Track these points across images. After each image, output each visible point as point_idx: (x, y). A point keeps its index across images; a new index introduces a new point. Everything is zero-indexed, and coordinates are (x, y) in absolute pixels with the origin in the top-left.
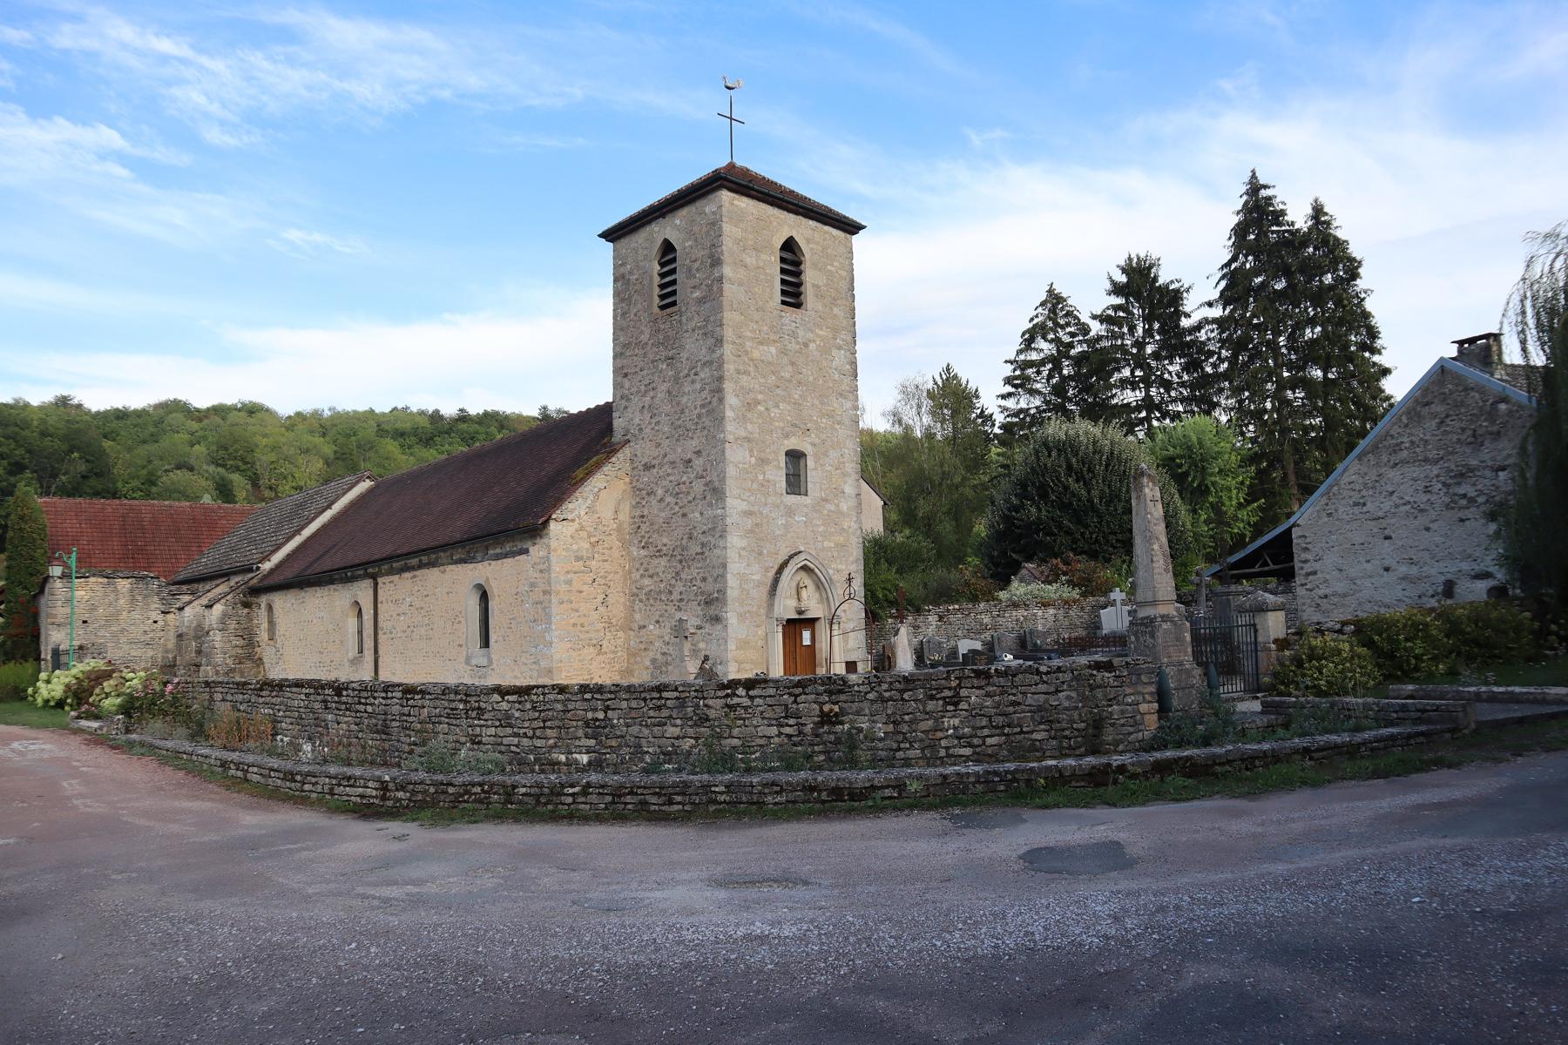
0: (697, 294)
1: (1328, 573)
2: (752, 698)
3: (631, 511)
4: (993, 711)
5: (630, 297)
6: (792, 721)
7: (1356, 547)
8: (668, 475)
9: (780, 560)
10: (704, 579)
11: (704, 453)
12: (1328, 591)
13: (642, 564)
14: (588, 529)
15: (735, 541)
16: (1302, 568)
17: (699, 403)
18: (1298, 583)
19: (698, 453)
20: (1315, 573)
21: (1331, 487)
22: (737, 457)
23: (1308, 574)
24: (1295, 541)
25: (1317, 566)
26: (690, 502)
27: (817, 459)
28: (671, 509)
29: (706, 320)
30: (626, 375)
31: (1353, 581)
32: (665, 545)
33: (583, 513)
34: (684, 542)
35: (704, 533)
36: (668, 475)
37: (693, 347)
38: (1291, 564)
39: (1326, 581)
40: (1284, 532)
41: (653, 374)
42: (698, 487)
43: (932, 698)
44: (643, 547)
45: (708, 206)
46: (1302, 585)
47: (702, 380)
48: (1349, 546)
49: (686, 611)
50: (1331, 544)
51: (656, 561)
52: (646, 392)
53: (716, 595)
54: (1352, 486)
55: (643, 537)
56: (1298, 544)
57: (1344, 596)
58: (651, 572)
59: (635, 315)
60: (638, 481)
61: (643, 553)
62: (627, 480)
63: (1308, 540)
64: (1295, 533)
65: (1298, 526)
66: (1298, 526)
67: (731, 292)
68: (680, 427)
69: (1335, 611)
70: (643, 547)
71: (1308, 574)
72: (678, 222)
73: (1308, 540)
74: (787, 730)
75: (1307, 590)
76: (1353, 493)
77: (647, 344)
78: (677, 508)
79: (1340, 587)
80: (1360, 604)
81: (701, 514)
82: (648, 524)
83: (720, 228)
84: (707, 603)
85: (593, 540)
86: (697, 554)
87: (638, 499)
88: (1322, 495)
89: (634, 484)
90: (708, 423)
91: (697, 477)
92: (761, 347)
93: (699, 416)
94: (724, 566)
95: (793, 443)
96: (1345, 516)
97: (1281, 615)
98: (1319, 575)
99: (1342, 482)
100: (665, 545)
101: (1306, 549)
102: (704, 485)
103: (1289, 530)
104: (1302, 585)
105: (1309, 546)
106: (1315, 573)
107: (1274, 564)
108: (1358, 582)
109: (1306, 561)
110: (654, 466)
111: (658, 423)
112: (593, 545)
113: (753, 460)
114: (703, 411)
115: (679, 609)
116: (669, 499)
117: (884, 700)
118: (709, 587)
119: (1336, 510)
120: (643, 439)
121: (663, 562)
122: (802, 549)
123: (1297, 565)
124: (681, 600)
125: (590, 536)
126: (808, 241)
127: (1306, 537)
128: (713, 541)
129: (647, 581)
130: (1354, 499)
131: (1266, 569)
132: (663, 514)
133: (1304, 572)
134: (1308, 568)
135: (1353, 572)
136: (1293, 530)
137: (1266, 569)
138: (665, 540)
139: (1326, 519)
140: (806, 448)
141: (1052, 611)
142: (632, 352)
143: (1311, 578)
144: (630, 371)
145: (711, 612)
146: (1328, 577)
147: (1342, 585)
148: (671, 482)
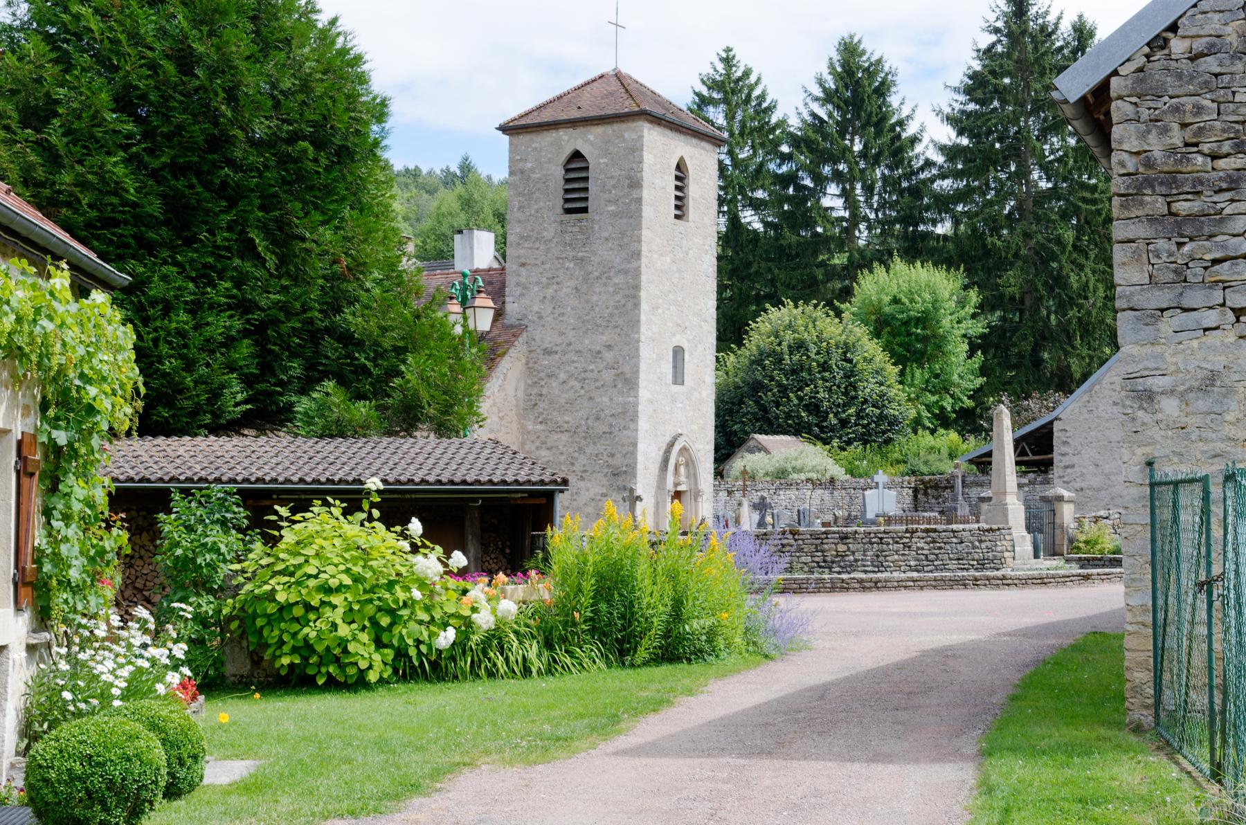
0: (612, 208)
1: (1085, 467)
2: (796, 540)
3: (526, 389)
4: (928, 552)
5: (531, 193)
6: (820, 554)
7: (1113, 445)
8: (573, 362)
9: (668, 439)
10: (612, 455)
11: (616, 348)
12: (1084, 485)
13: (538, 437)
14: (499, 405)
15: (643, 424)
16: (1061, 461)
17: (611, 303)
18: (1056, 475)
19: (609, 347)
20: (1073, 466)
21: (1093, 385)
22: (646, 352)
23: (1066, 467)
24: (1055, 434)
25: (1075, 460)
26: (597, 388)
27: (691, 354)
28: (576, 391)
29: (623, 234)
30: (523, 265)
31: (1107, 476)
32: (566, 423)
33: (496, 391)
34: (590, 422)
35: (613, 415)
36: (573, 362)
37: (603, 252)
38: (1050, 456)
39: (1082, 475)
40: (1043, 427)
41: (557, 270)
42: (608, 376)
43: (897, 543)
44: (541, 423)
45: (628, 131)
46: (1060, 477)
47: (615, 284)
48: (1106, 443)
49: (590, 480)
50: (1090, 440)
51: (556, 437)
52: (548, 284)
53: (624, 469)
54: (1113, 386)
55: (542, 413)
56: (1059, 438)
57: (1099, 490)
58: (549, 445)
59: (537, 211)
60: (535, 363)
61: (539, 427)
62: (524, 361)
63: (1068, 434)
64: (1057, 426)
65: (1060, 419)
66: (1060, 419)
67: (647, 211)
68: (588, 322)
69: (1089, 504)
70: (541, 423)
71: (1066, 467)
72: (591, 137)
73: (1068, 434)
74: (816, 559)
75: (1064, 482)
76: (1113, 393)
77: (550, 241)
78: (582, 392)
79: (1095, 481)
80: (1112, 499)
81: (611, 400)
82: (546, 402)
83: (641, 156)
84: (614, 475)
85: (501, 414)
86: (604, 433)
87: (535, 380)
88: (1086, 392)
89: (531, 365)
90: (621, 323)
91: (606, 368)
92: (663, 258)
93: (611, 315)
94: (635, 445)
95: (679, 340)
96: (1104, 414)
97: (1072, 506)
98: (1076, 469)
99: (1104, 382)
100: (566, 423)
101: (1065, 443)
102: (615, 375)
103: (1051, 423)
104: (1060, 477)
105: (1069, 440)
106: (1073, 466)
107: (1033, 454)
108: (1111, 477)
109: (1064, 455)
110: (556, 353)
111: (562, 314)
112: (501, 418)
113: (655, 356)
114: (616, 311)
115: (582, 478)
116: (572, 383)
117: (872, 543)
118: (617, 461)
119: (1097, 408)
120: (543, 326)
121: (565, 437)
122: (680, 431)
123: (1056, 456)
124: (585, 471)
125: (499, 411)
126: (691, 158)
127: (1066, 431)
128: (623, 423)
129: (544, 453)
130: (1113, 399)
131: (1026, 458)
132: (565, 396)
133: (1062, 465)
134: (1067, 461)
135: (1108, 468)
136: (1055, 423)
137: (1026, 458)
138: (567, 418)
139: (1087, 416)
140: (686, 346)
141: (819, 492)
142: (531, 245)
143: (1069, 471)
144: (528, 262)
145: (619, 483)
146: (1084, 471)
147: (1097, 479)
148: (576, 368)
